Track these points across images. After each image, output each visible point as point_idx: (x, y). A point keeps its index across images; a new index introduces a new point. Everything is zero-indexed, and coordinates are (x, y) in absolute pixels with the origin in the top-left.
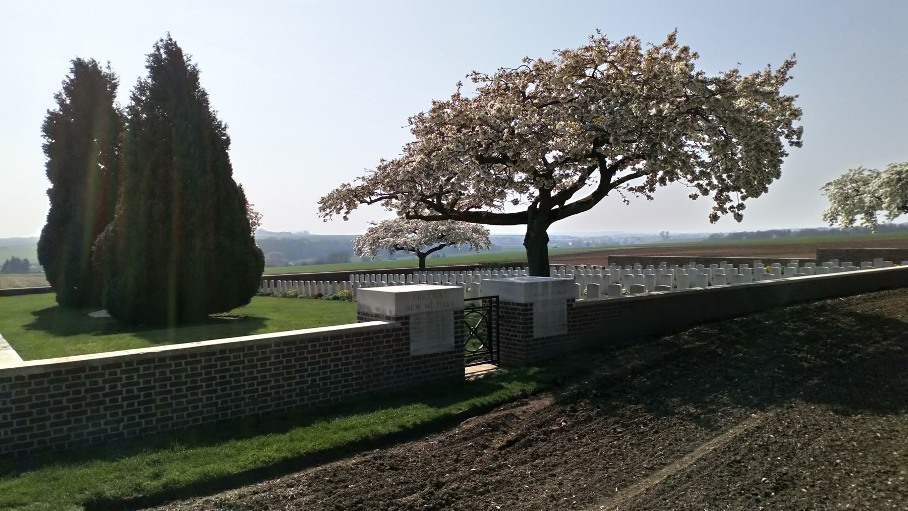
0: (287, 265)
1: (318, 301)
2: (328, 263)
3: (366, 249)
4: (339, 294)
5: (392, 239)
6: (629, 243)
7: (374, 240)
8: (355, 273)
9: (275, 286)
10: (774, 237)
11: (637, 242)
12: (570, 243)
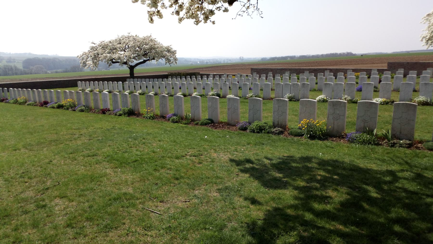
0: (46, 73)
1: (43, 110)
2: (71, 72)
3: (90, 62)
4: (63, 102)
5: (109, 55)
6: (226, 62)
7: (95, 56)
8: (81, 80)
9: (8, 91)
10: (289, 59)
11: (229, 62)
12: (199, 62)
